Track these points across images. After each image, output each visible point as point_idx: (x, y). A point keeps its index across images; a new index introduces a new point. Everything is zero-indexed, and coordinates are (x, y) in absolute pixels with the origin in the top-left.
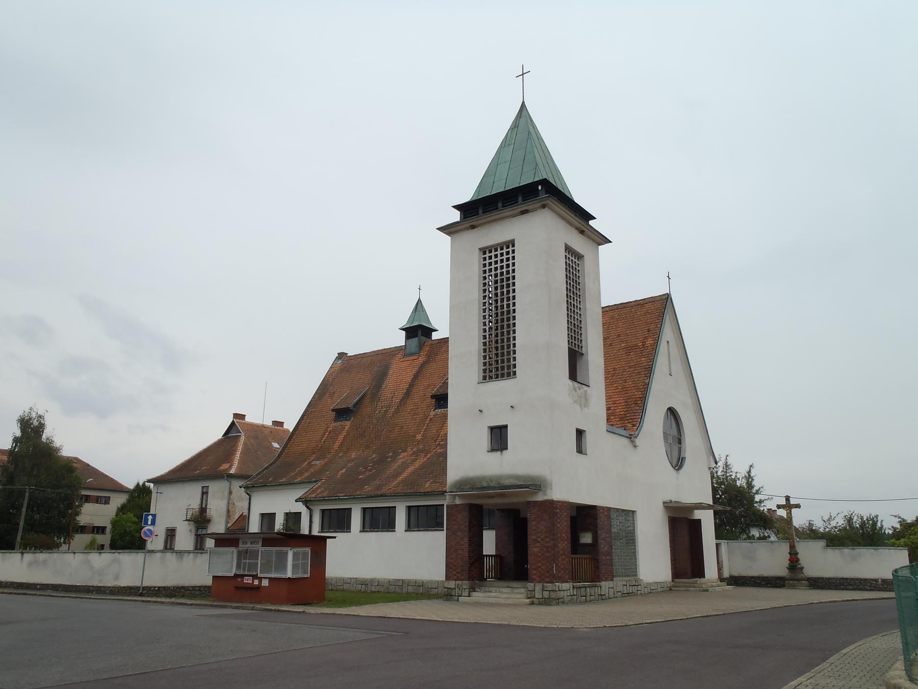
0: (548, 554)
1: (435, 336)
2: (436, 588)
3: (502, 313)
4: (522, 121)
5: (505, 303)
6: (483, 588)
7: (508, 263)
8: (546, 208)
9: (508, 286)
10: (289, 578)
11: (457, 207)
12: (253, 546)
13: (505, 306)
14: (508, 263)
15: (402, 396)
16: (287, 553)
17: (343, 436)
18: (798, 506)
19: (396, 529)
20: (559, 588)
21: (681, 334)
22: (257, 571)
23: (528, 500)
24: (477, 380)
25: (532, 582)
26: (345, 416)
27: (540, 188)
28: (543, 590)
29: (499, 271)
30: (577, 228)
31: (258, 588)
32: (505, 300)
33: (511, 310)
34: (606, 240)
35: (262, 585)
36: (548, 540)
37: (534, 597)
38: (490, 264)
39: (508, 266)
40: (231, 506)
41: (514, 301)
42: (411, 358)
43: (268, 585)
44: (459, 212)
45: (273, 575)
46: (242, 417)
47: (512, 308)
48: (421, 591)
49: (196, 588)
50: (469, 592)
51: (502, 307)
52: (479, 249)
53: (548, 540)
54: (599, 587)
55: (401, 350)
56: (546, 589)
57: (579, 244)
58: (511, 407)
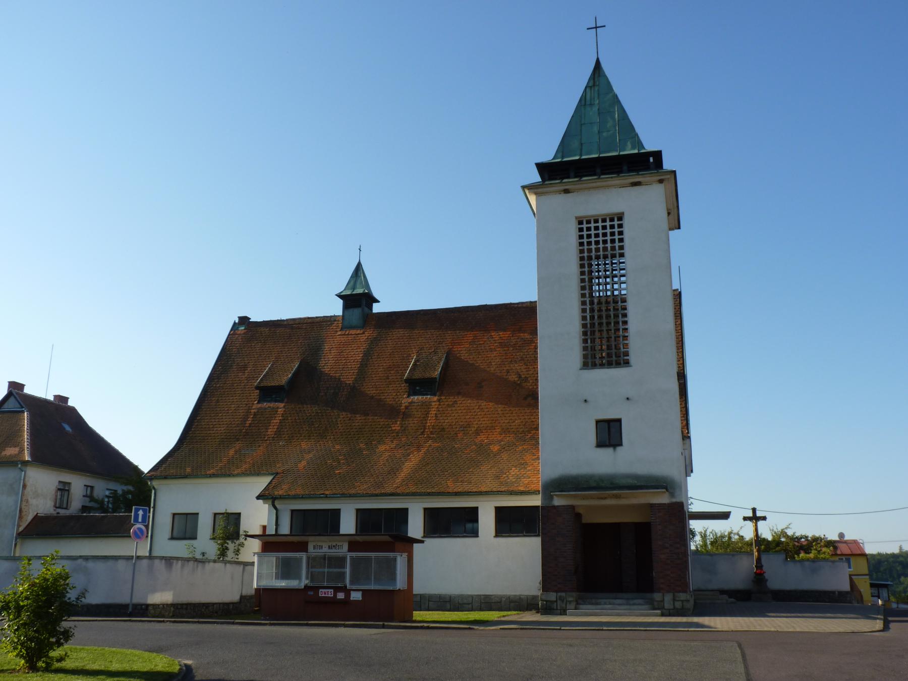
1: (377, 308)
2: (469, 604)
15: (353, 377)
16: (395, 560)
17: (278, 421)
18: (764, 518)
19: (479, 535)
23: (651, 502)
24: (579, 368)
26: (274, 396)
27: (651, 160)
28: (674, 600)
30: (560, 192)
31: (347, 601)
35: (351, 599)
39: (613, 241)
40: (24, 503)
42: (353, 332)
45: (373, 587)
56: (677, 599)
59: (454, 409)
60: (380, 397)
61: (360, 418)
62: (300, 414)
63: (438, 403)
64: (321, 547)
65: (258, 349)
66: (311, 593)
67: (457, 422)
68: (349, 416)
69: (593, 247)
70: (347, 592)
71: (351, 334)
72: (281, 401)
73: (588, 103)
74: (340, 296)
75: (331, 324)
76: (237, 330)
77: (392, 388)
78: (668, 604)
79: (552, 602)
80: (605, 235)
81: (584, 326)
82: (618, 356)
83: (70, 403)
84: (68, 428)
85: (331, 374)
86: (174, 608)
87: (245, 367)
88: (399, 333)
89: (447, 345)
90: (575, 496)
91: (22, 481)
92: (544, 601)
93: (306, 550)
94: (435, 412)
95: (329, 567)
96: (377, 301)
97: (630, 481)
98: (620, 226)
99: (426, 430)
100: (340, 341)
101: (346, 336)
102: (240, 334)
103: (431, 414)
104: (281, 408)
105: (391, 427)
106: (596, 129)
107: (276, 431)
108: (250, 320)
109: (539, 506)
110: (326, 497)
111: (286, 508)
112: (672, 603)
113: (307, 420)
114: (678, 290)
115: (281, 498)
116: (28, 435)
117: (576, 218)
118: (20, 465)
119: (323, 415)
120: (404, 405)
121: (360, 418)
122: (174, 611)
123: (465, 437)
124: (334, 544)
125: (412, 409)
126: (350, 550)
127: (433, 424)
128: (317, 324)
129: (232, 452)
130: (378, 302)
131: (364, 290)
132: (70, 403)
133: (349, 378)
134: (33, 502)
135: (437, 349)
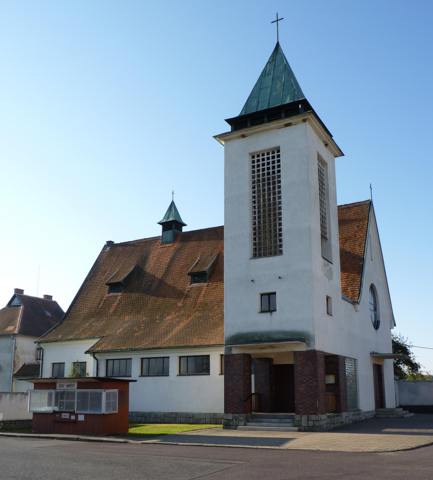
0: (312, 392)
1: (185, 229)
3: (269, 205)
4: (278, 56)
5: (272, 196)
6: (255, 419)
7: (269, 166)
8: (307, 122)
9: (274, 183)
10: (104, 414)
11: (229, 121)
12: (68, 388)
13: (272, 199)
14: (269, 166)
15: (162, 274)
16: (101, 394)
17: (116, 304)
20: (320, 419)
21: (378, 231)
22: (74, 408)
23: (294, 350)
25: (299, 414)
26: (117, 289)
27: (300, 106)
28: (308, 420)
29: (266, 172)
30: (324, 142)
31: (76, 422)
32: (272, 194)
33: (277, 202)
34: (340, 153)
35: (79, 420)
36: (312, 381)
37: (301, 425)
38: (258, 166)
39: (274, 167)
40: (16, 358)
41: (280, 195)
42: (167, 245)
43: (84, 420)
44: (230, 127)
45: (88, 412)
46: (22, 291)
47: (277, 200)
48: (192, 421)
49: (13, 422)
50: (245, 422)
51: (269, 199)
52: (249, 153)
53: (312, 381)
54: (341, 417)
55: (159, 239)
56: (310, 419)
57: (326, 154)
58: (252, 281)
59: (215, 290)
60: (175, 286)
61: (161, 300)
62: (129, 299)
63: (207, 287)
64: (63, 386)
65: (114, 260)
66: (58, 416)
67: (216, 299)
68: (155, 298)
69: (261, 173)
70: (77, 415)
71: (166, 247)
72: (120, 292)
73: (267, 74)
74: (160, 223)
75: (156, 242)
76: (105, 249)
77: (183, 279)
78: (304, 423)
79: (230, 420)
80: (268, 163)
81: (255, 229)
82: (275, 247)
83: (54, 299)
84: (48, 314)
85: (150, 273)
86: (3, 423)
87: (106, 271)
88: (193, 244)
89: (219, 249)
90: (245, 348)
91: (14, 345)
92: (225, 419)
93: (55, 389)
94: (204, 293)
95: (67, 399)
96: (185, 225)
97: (281, 336)
98: (279, 156)
99: (197, 305)
100: (159, 252)
101: (163, 248)
102: (107, 252)
103: (202, 294)
104: (119, 296)
105: (177, 304)
106: (269, 90)
107: (114, 311)
108: (114, 243)
109: (223, 355)
110: (122, 351)
111: (103, 358)
112: (307, 422)
113: (132, 302)
114: (370, 200)
115: (98, 352)
116: (20, 319)
117: (250, 154)
118: (12, 336)
119: (141, 299)
120: (187, 290)
121: (161, 300)
122: (3, 425)
123: (218, 309)
124: (70, 384)
125: (191, 292)
126: (78, 388)
127: (201, 301)
128: (148, 242)
129: (87, 324)
130: (186, 225)
131: (173, 219)
132: (54, 299)
133: (159, 275)
134: (21, 357)
135: (212, 252)
